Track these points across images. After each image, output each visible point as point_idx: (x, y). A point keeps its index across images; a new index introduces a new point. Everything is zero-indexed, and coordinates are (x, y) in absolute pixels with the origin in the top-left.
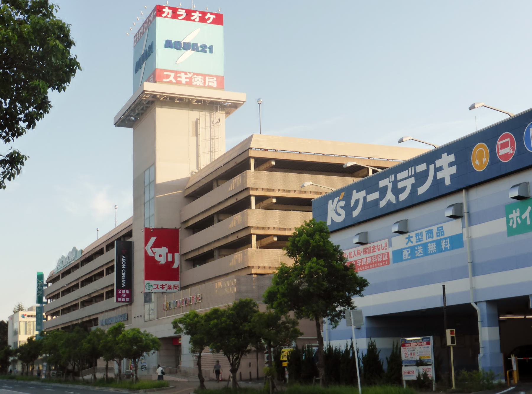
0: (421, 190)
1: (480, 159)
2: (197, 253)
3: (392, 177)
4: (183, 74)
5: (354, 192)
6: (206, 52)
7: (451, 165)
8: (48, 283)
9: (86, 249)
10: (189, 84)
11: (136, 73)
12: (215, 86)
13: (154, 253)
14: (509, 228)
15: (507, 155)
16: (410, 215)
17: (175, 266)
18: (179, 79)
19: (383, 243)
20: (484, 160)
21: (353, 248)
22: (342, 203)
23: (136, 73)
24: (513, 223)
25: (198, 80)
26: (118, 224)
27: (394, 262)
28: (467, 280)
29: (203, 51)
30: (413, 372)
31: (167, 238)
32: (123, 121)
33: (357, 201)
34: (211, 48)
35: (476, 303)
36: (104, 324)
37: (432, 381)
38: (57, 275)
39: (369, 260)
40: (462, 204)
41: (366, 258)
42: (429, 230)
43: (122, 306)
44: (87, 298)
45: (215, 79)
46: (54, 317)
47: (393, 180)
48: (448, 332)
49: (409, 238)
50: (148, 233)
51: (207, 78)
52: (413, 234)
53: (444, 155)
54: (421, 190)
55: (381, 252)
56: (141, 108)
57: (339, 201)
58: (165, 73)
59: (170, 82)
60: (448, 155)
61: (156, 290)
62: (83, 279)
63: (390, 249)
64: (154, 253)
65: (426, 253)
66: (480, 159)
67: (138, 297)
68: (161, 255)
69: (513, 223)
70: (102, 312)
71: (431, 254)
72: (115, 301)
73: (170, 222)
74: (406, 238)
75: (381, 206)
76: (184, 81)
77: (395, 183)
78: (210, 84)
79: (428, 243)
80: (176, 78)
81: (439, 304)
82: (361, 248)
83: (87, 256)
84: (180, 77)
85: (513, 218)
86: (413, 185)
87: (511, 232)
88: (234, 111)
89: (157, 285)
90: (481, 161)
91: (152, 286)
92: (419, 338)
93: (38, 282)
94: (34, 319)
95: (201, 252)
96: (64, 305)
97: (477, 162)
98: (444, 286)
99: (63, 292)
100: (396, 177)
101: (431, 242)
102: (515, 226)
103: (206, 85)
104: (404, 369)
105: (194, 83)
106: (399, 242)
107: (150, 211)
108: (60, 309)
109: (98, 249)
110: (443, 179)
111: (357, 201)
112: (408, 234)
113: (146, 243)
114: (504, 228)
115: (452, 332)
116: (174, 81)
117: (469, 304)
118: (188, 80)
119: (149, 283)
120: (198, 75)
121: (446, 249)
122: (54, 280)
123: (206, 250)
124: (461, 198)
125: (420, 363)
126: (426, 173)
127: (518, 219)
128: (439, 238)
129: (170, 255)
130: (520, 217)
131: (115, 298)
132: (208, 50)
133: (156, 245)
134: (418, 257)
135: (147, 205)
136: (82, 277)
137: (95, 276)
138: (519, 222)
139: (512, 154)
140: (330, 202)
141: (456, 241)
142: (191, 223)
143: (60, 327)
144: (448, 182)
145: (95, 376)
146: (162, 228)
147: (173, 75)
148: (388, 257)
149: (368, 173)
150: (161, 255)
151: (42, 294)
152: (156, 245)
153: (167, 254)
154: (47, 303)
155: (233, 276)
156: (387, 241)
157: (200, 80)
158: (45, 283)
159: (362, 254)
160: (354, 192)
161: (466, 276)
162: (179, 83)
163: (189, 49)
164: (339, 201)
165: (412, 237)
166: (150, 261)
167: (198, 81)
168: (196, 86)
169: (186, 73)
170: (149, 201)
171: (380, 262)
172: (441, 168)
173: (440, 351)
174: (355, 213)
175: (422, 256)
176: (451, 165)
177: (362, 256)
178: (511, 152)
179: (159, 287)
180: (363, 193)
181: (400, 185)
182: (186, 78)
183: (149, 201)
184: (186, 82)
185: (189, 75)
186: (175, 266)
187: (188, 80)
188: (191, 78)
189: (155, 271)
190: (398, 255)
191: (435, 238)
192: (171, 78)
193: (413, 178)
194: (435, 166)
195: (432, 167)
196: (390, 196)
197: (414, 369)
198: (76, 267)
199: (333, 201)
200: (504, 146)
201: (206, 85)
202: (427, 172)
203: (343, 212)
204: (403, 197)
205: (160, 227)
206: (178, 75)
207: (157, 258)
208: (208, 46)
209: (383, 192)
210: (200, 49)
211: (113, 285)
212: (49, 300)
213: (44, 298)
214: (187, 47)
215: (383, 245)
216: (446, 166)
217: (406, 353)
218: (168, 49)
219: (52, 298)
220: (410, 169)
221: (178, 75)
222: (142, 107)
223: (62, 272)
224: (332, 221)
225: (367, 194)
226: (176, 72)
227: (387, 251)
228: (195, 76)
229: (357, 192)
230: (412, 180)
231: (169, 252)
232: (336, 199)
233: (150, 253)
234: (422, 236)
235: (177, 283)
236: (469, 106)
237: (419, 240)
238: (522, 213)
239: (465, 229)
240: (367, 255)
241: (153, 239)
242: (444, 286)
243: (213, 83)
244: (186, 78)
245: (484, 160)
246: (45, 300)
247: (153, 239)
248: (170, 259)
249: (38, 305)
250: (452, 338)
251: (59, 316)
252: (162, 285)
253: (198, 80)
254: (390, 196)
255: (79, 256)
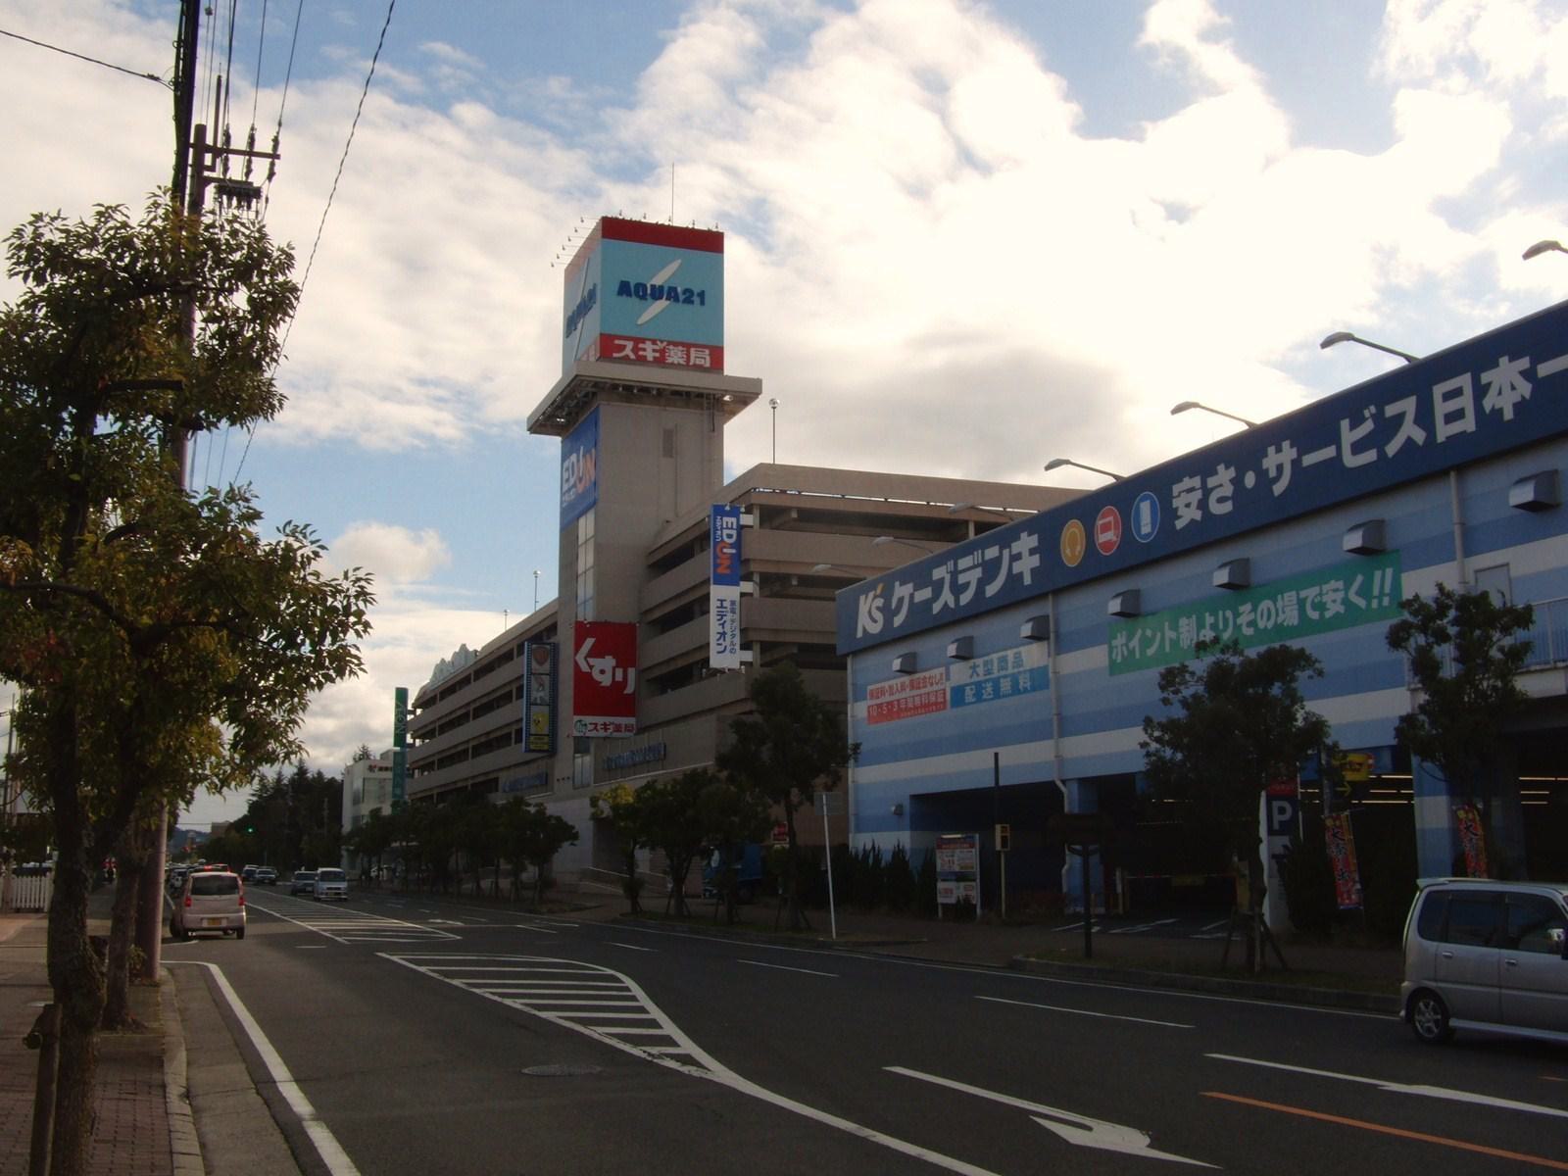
0: (991, 590)
1: (1072, 545)
2: (664, 670)
3: (951, 564)
4: (648, 343)
5: (897, 584)
6: (692, 302)
7: (1032, 552)
8: (415, 706)
9: (483, 649)
10: (661, 361)
11: (567, 337)
12: (708, 365)
13: (591, 667)
14: (1112, 663)
15: (1107, 545)
16: (977, 630)
17: (629, 690)
18: (641, 353)
19: (936, 672)
20: (1079, 548)
21: (895, 678)
22: (880, 602)
23: (567, 337)
24: (1117, 654)
25: (676, 354)
26: (508, 628)
27: (952, 706)
28: (1049, 744)
29: (688, 301)
30: (951, 891)
31: (612, 638)
32: (703, 292)
33: (901, 600)
34: (702, 295)
35: (1064, 782)
36: (507, 789)
37: (975, 906)
38: (432, 695)
39: (917, 701)
40: (1048, 616)
41: (913, 697)
42: (1003, 657)
43: (543, 757)
44: (483, 740)
45: (707, 352)
46: (426, 773)
47: (952, 569)
48: (998, 827)
49: (974, 667)
50: (582, 631)
51: (692, 350)
52: (979, 661)
53: (1024, 535)
54: (991, 590)
55: (935, 688)
56: (573, 403)
57: (875, 597)
58: (617, 342)
59: (626, 360)
60: (1510, 361)
61: (593, 734)
62: (478, 704)
63: (948, 684)
64: (591, 667)
65: (997, 694)
66: (1072, 545)
67: (566, 747)
68: (604, 670)
69: (1117, 654)
70: (509, 768)
71: (1004, 696)
72: (523, 749)
73: (623, 612)
74: (971, 667)
75: (935, 612)
76: (650, 355)
77: (955, 574)
78: (698, 362)
79: (999, 678)
80: (635, 350)
81: (988, 782)
82: (906, 679)
83: (485, 662)
84: (644, 350)
85: (1116, 647)
86: (980, 581)
87: (1114, 668)
88: (742, 409)
89: (596, 724)
90: (1073, 551)
91: (586, 725)
92: (959, 836)
93: (397, 706)
94: (389, 775)
95: (672, 667)
96: (443, 751)
97: (1068, 551)
98: (996, 755)
99: (441, 727)
100: (956, 565)
101: (1005, 677)
102: (1119, 660)
103: (691, 364)
104: (941, 885)
105: (670, 360)
106: (960, 673)
107: (586, 589)
108: (436, 758)
109: (505, 650)
110: (1021, 575)
111: (901, 600)
112: (972, 661)
113: (578, 646)
114: (1106, 662)
115: (1004, 829)
116: (633, 356)
117: (1052, 784)
118: (657, 355)
119: (580, 721)
120: (676, 344)
121: (1026, 690)
122: (426, 700)
123: (680, 663)
124: (1046, 608)
125: (961, 877)
126: (998, 560)
127: (1124, 648)
128: (1016, 670)
129: (619, 674)
130: (1127, 645)
131: (524, 744)
132: (696, 299)
133: (595, 653)
134: (985, 700)
135: (581, 580)
136: (475, 700)
137: (459, 717)
138: (1126, 653)
139: (1115, 542)
140: (862, 598)
141: (1040, 679)
142: (657, 614)
143: (435, 792)
144: (1027, 580)
145: (478, 886)
146: (606, 622)
147: (630, 345)
148: (944, 698)
149: (967, 533)
150: (604, 670)
151: (404, 730)
152: (595, 653)
153: (614, 669)
154: (412, 745)
155: (713, 717)
156: (942, 670)
157: (680, 354)
158: (410, 707)
159: (908, 690)
160: (897, 584)
161: (1049, 736)
162: (641, 360)
163: (661, 298)
164: (875, 597)
165: (978, 666)
166: (583, 680)
167: (676, 356)
168: (672, 365)
169: (654, 342)
170: (585, 573)
171: (932, 704)
172: (1016, 557)
173: (988, 858)
174: (898, 621)
175: (992, 699)
176: (1032, 552)
177: (908, 693)
178: (1114, 539)
179: (599, 728)
180: (910, 587)
181: (962, 579)
182: (654, 351)
183: (585, 573)
184: (655, 358)
185: (660, 346)
186: (629, 690)
187: (657, 355)
188: (663, 352)
189: (591, 697)
190: (958, 693)
191: (1010, 671)
192: (628, 351)
193: (979, 570)
194: (1010, 552)
195: (1006, 553)
196: (947, 597)
197: (951, 885)
198: (465, 681)
199: (866, 597)
200: (1106, 528)
201: (691, 364)
202: (998, 560)
203: (878, 616)
204: (965, 598)
205: (603, 621)
206: (641, 346)
207: (597, 676)
208: (696, 291)
209: (938, 587)
210: (682, 297)
211: (521, 719)
212: (417, 741)
213: (409, 736)
214: (657, 293)
215: (938, 677)
216: (1025, 553)
217: (943, 860)
218: (624, 298)
219: (422, 737)
220: (976, 553)
221: (641, 346)
222: (575, 401)
223: (474, 668)
224: (865, 630)
225: (1535, 362)
226: (637, 341)
227: (942, 687)
228: (671, 347)
229: (901, 585)
230: (978, 573)
231: (618, 666)
232: (871, 595)
233: (585, 668)
234: (992, 665)
235: (631, 721)
236: (1173, 407)
237: (988, 672)
238: (1129, 638)
239: (1051, 659)
240: (916, 692)
241: (589, 642)
242: (996, 755)
243: (703, 360)
244: (654, 351)
245: (1079, 548)
246: (409, 740)
247: (589, 642)
248: (619, 677)
249: (398, 749)
250: (1004, 840)
251: (433, 770)
252: (605, 724)
253: (676, 354)
254: (947, 597)
255: (471, 662)
